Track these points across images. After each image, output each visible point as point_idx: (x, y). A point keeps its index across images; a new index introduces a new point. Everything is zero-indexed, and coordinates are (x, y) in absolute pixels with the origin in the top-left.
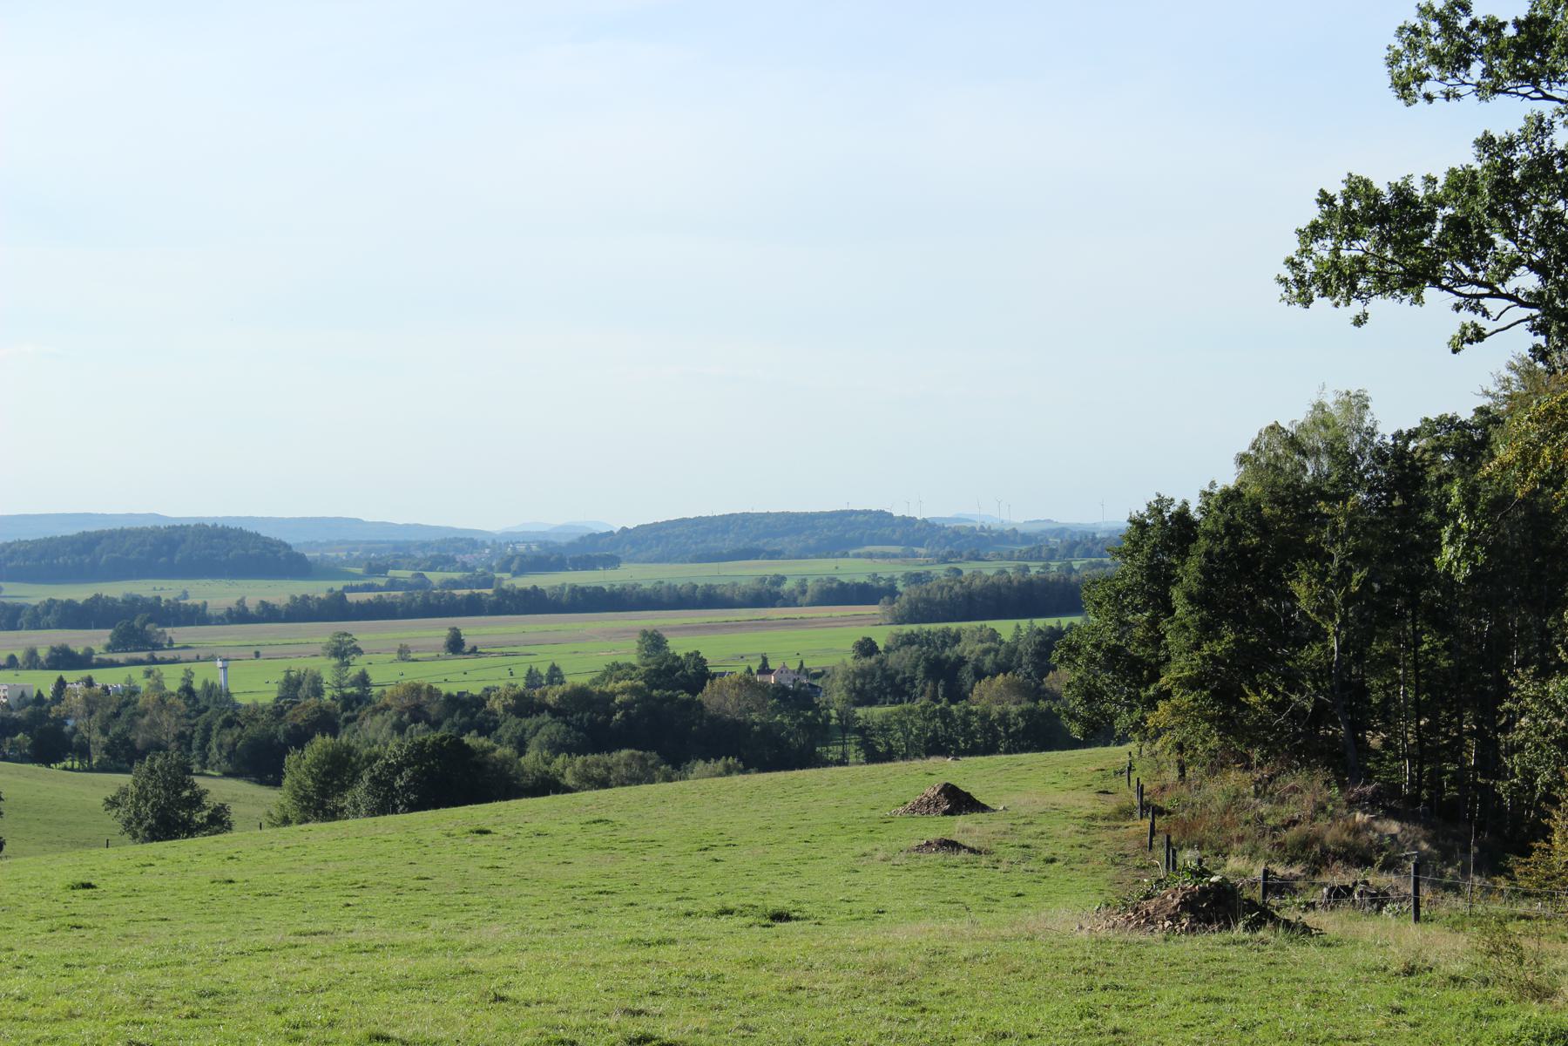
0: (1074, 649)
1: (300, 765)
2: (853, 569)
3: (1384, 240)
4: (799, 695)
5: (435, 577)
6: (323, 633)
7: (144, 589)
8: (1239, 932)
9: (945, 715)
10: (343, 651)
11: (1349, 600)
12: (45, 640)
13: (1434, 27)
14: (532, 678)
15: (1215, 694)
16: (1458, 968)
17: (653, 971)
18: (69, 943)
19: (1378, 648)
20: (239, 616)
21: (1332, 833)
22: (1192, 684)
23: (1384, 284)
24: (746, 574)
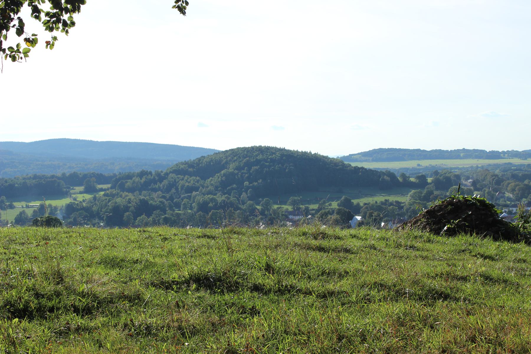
3: (190, 226)
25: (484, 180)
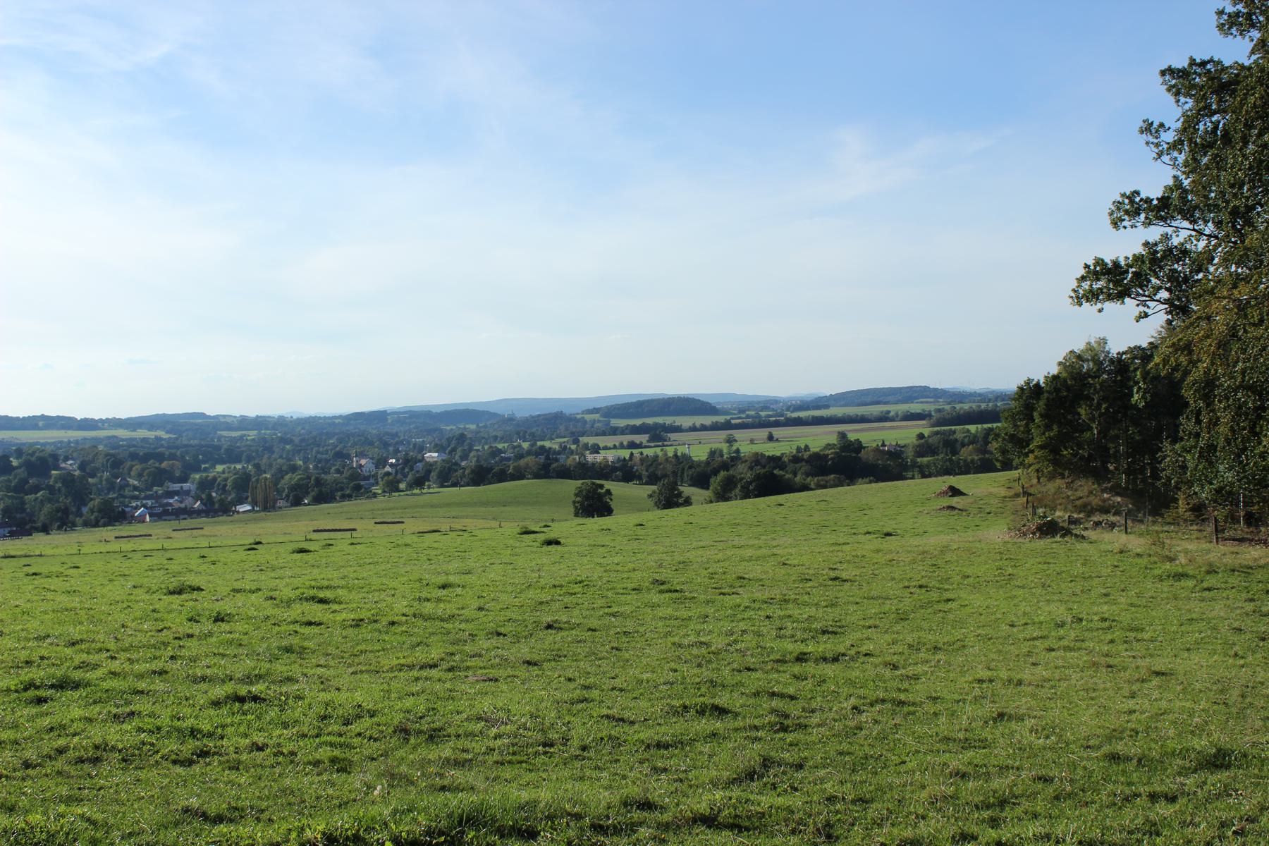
0: (997, 435)
1: (716, 481)
2: (916, 408)
3: (1109, 281)
4: (896, 453)
5: (763, 414)
6: (723, 434)
7: (660, 420)
8: (1058, 538)
9: (950, 460)
10: (730, 441)
11: (1101, 415)
12: (626, 439)
13: (1127, 201)
14: (799, 449)
15: (1051, 451)
16: (1139, 550)
17: (840, 554)
18: (635, 544)
19: (1112, 433)
20: (693, 429)
21: (1095, 501)
22: (1041, 447)
23: (1110, 297)
24: (876, 410)
25: (93, 461)
